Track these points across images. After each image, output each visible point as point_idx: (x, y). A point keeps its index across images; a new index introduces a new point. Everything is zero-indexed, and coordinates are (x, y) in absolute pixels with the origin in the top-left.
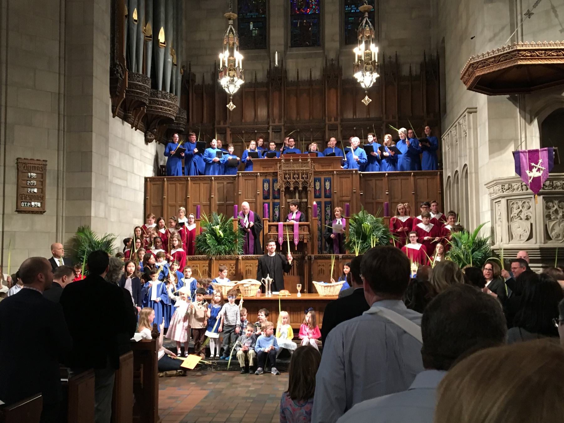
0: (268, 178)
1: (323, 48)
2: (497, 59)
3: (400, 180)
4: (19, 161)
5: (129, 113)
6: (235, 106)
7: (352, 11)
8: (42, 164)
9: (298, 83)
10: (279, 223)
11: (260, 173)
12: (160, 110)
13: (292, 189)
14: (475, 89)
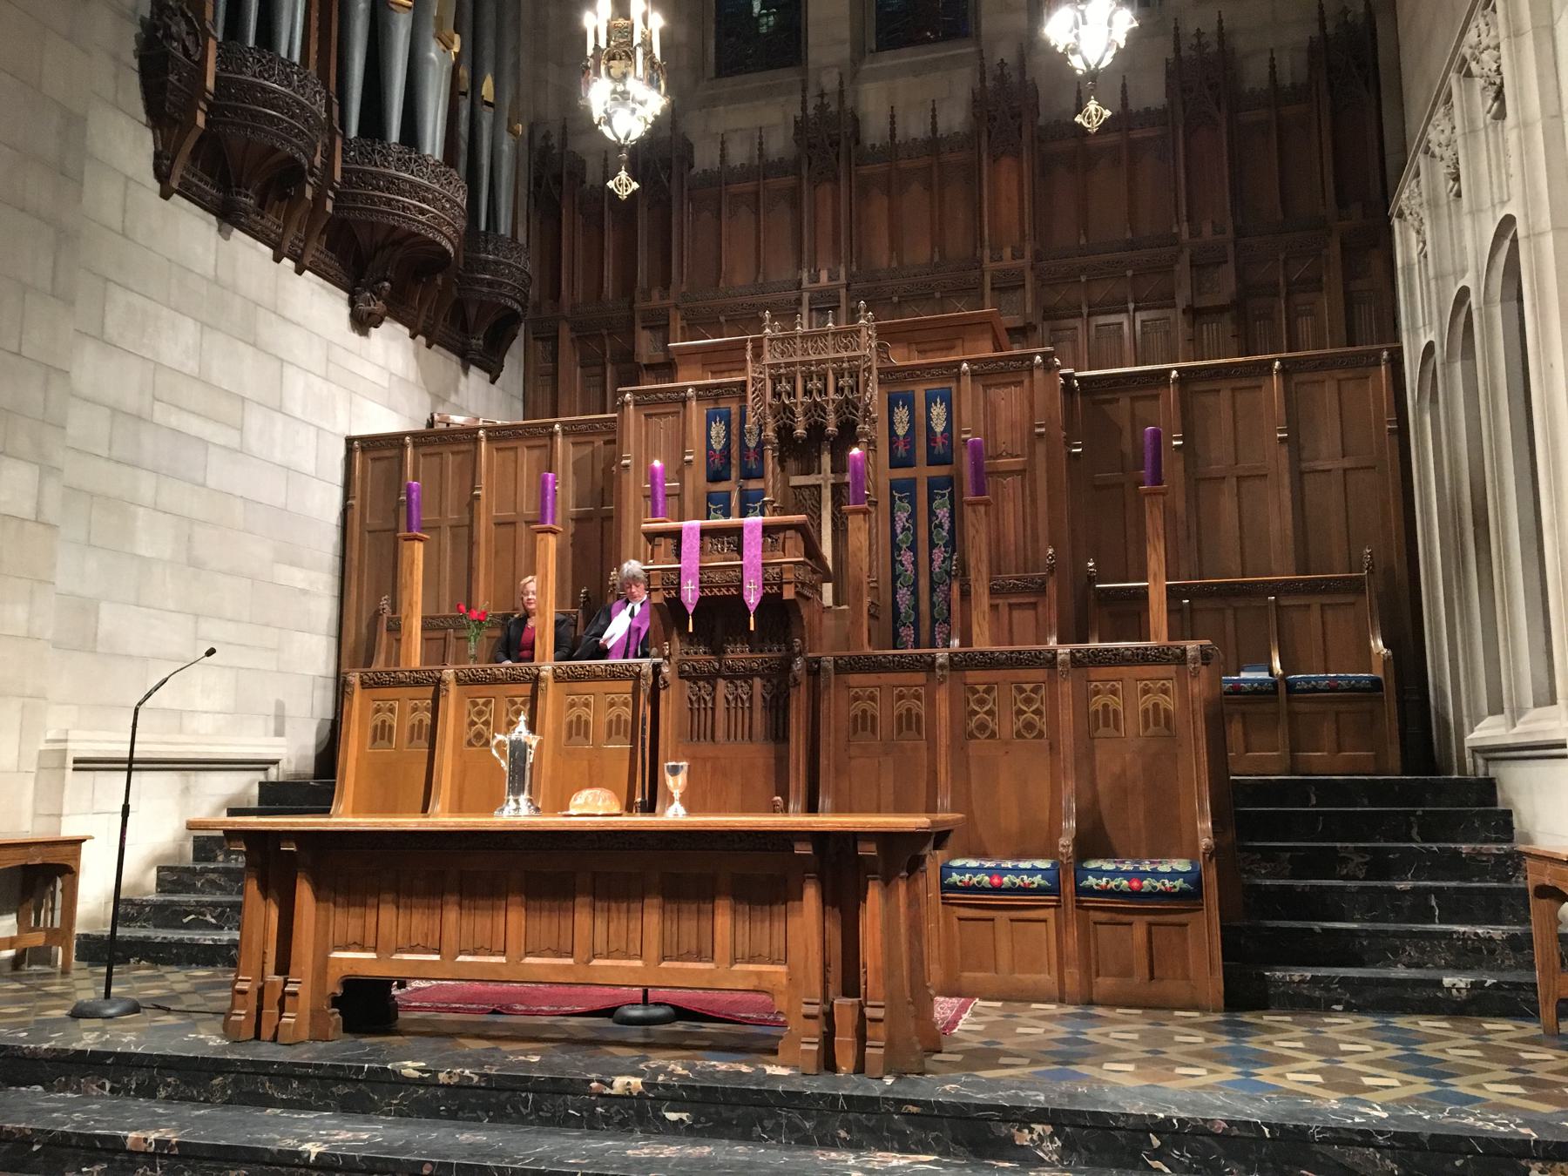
0: (723, 405)
3: (1225, 395)
5: (239, 193)
6: (635, 186)
9: (892, 149)
10: (685, 524)
11: (697, 388)
12: (384, 208)
13: (800, 431)
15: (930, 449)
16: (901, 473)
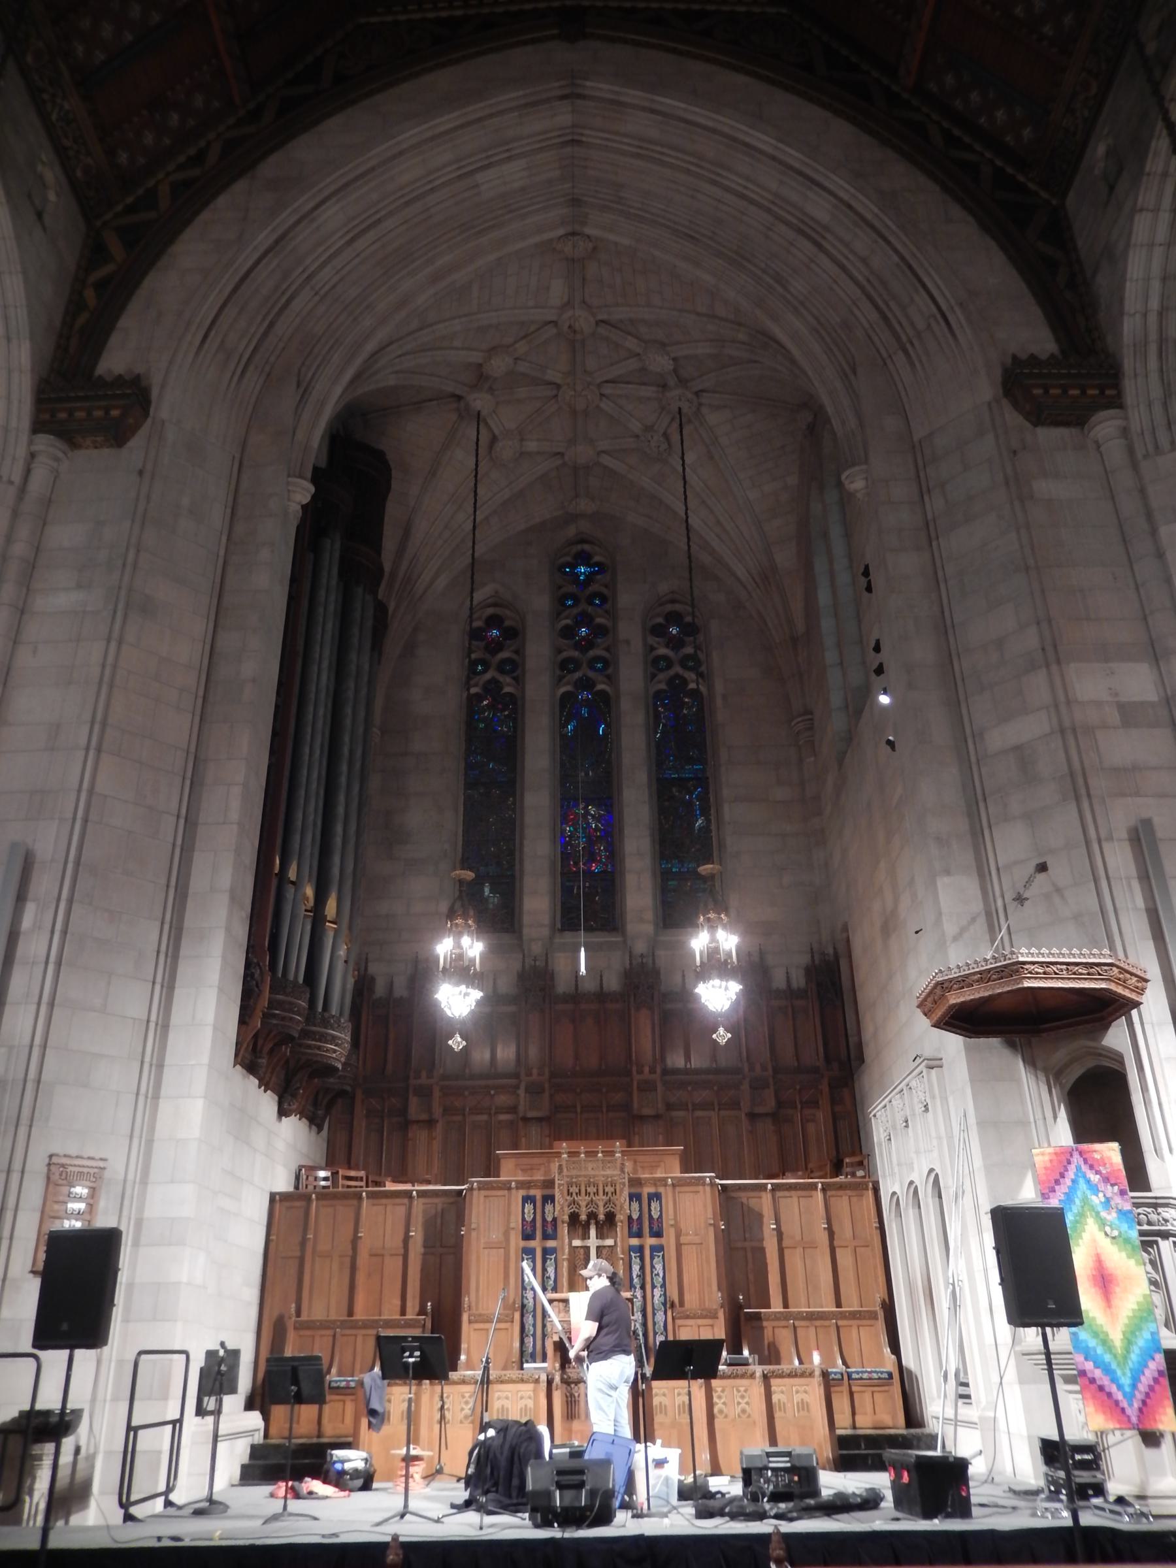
1: (624, 933)
2: (985, 976)
4: (54, 1160)
7: (674, 870)
8: (96, 1168)
14: (944, 1027)
15: (651, 1228)
16: (635, 1242)
